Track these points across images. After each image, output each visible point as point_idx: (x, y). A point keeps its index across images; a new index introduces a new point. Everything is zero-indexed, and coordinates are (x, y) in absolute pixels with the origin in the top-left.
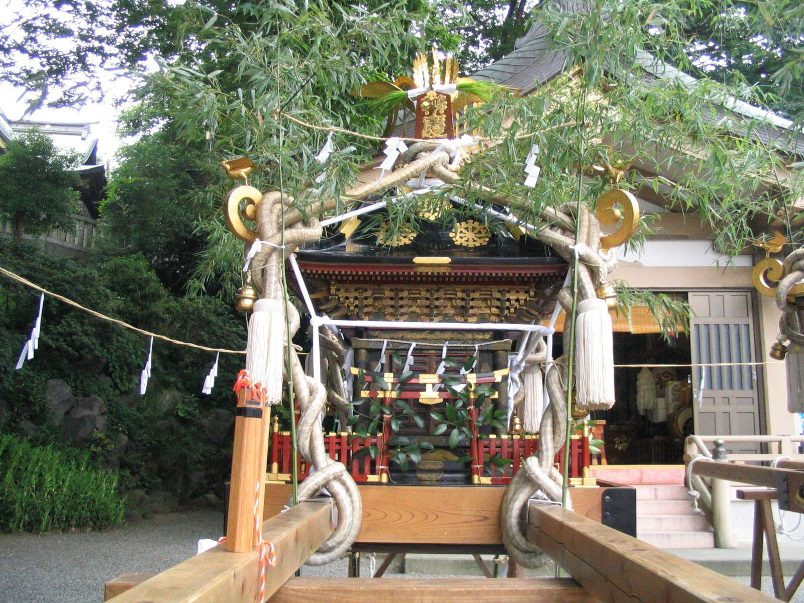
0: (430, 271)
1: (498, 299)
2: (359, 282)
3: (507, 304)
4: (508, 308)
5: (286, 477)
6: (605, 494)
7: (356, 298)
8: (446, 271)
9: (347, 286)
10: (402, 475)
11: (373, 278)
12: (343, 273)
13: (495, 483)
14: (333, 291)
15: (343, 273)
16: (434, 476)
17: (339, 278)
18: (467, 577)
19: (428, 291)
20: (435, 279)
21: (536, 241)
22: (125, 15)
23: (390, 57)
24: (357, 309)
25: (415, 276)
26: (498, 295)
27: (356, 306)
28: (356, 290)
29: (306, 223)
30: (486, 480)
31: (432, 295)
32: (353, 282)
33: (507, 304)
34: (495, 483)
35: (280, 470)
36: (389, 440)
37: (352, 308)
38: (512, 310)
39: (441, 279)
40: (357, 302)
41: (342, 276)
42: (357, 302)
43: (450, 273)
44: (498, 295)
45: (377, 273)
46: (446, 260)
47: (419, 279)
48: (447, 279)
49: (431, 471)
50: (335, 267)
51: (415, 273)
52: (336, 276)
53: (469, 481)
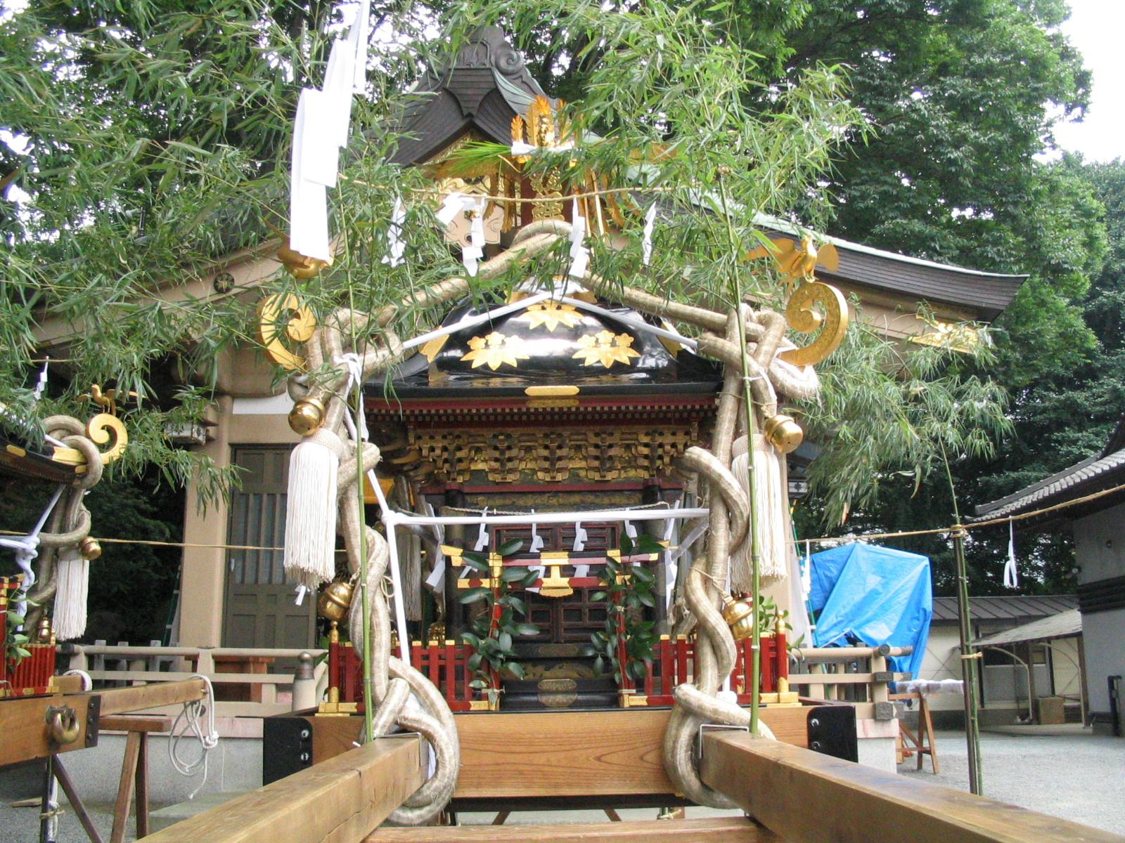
0: (549, 404)
1: (646, 445)
2: (448, 424)
3: (660, 451)
4: (661, 457)
5: (351, 707)
6: (811, 715)
7: (445, 449)
8: (573, 404)
9: (431, 431)
10: (515, 698)
11: (444, 419)
12: (425, 412)
13: (652, 704)
14: (412, 440)
15: (433, 412)
16: (560, 698)
17: (420, 419)
18: (636, 832)
19: (597, 435)
20: (572, 417)
21: (696, 359)
22: (11, 30)
23: (983, 256)
24: (447, 466)
25: (528, 413)
26: (646, 440)
27: (446, 461)
28: (444, 437)
29: (380, 341)
30: (641, 700)
31: (603, 440)
32: (440, 424)
33: (660, 451)
34: (652, 704)
35: (342, 698)
36: (498, 645)
37: (440, 463)
38: (667, 460)
39: (572, 417)
40: (446, 455)
41: (424, 416)
42: (446, 455)
43: (578, 408)
44: (646, 440)
45: (441, 412)
46: (572, 390)
47: (524, 418)
48: (548, 418)
49: (557, 692)
50: (427, 404)
51: (528, 409)
52: (416, 417)
53: (614, 703)
